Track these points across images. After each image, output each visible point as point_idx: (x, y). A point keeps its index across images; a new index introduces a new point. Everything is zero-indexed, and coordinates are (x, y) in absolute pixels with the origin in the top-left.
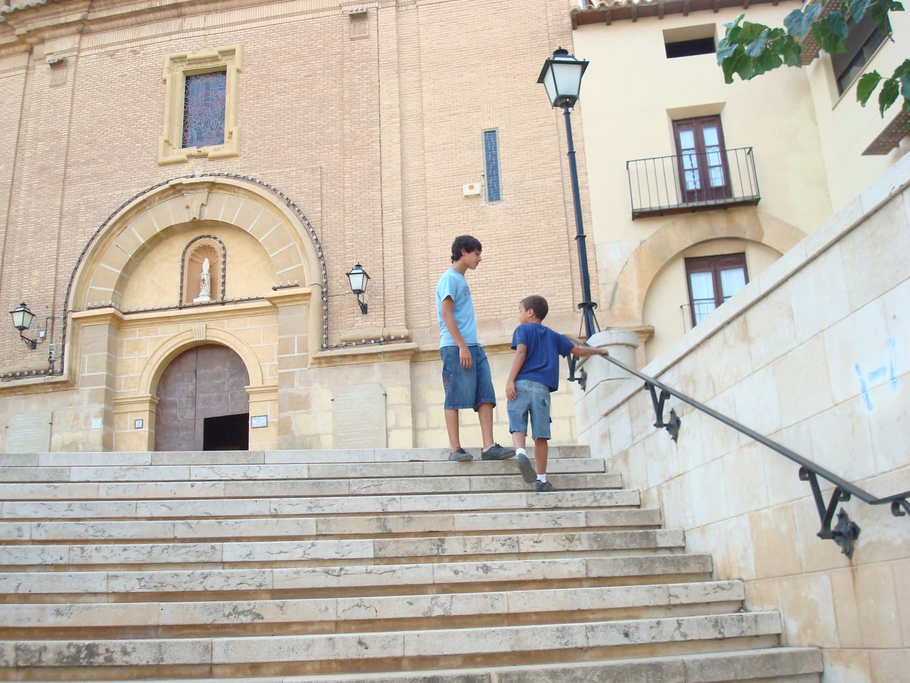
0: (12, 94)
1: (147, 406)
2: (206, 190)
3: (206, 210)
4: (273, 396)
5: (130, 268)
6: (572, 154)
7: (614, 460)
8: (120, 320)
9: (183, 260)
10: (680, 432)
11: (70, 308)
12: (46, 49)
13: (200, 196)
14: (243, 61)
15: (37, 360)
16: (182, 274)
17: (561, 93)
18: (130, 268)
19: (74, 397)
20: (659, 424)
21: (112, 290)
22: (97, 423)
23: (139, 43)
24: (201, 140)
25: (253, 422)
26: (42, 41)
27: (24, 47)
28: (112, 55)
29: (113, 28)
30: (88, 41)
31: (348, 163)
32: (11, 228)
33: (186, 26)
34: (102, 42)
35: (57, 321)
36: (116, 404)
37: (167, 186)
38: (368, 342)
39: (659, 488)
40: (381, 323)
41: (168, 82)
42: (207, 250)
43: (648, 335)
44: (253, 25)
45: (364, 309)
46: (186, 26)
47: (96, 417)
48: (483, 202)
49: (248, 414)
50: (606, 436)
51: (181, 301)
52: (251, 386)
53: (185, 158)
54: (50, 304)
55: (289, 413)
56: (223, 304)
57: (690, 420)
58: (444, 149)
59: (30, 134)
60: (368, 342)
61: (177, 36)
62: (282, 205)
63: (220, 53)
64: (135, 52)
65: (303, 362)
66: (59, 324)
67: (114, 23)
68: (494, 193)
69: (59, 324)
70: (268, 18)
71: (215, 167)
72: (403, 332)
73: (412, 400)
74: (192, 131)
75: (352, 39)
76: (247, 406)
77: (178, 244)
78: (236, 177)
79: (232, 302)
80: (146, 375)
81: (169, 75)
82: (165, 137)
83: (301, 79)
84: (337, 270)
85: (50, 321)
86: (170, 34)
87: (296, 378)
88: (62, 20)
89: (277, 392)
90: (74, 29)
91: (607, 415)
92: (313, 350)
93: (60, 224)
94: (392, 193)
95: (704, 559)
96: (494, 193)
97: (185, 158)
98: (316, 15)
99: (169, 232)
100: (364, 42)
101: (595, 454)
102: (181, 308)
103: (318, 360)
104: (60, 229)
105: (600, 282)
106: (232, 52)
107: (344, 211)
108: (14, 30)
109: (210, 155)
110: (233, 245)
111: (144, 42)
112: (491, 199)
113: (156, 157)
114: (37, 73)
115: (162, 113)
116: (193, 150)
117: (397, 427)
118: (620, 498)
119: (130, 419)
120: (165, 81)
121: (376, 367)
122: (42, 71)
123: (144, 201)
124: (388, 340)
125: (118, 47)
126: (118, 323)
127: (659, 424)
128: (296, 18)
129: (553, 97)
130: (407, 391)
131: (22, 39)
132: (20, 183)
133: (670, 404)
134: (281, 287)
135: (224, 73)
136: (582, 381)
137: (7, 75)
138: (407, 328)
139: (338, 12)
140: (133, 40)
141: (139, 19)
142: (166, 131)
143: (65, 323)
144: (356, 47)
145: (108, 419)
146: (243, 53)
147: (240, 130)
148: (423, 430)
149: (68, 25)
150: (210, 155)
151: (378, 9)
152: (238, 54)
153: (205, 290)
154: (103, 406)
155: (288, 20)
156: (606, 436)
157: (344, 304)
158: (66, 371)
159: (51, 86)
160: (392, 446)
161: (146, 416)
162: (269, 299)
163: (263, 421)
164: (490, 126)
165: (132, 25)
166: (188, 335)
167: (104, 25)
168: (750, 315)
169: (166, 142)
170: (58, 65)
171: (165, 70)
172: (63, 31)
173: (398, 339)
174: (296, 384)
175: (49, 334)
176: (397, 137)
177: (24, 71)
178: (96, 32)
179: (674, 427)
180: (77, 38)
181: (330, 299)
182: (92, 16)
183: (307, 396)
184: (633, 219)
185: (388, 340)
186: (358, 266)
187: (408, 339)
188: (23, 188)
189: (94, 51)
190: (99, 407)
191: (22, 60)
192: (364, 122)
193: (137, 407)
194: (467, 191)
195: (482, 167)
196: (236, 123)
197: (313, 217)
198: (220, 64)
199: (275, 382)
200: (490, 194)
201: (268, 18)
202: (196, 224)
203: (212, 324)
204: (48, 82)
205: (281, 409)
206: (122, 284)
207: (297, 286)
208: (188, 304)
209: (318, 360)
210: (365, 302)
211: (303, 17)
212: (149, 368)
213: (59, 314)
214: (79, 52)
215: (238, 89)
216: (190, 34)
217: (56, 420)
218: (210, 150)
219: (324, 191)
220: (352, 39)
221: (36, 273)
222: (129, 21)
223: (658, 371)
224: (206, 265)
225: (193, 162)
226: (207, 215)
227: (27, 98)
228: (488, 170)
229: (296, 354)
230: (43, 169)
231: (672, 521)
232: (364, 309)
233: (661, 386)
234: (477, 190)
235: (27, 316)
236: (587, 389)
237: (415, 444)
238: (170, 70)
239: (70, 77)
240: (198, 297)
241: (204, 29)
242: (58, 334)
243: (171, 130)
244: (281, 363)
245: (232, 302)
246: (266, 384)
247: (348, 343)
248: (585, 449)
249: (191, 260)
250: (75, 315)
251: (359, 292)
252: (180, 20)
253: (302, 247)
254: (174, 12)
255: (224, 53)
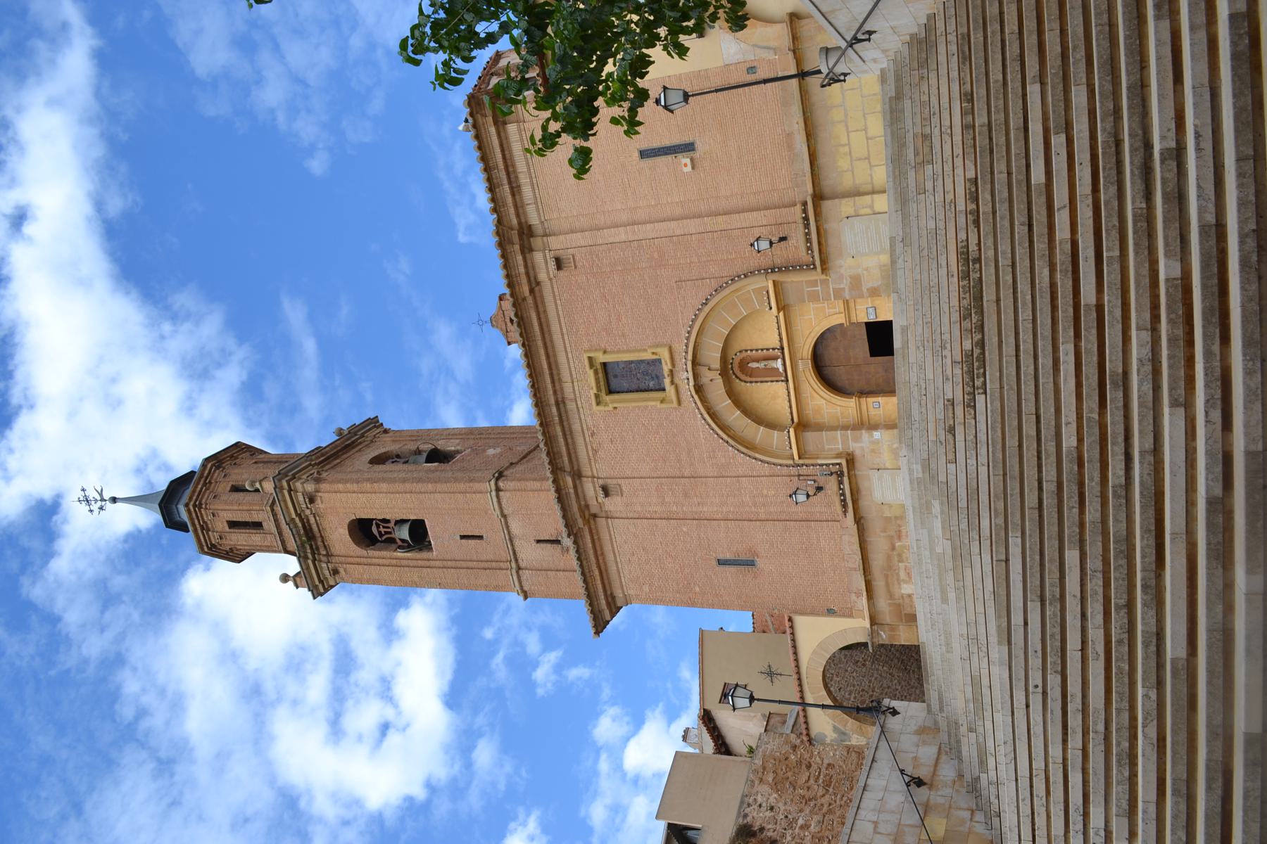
0: (628, 528)
1: (863, 400)
2: (698, 367)
3: (713, 366)
4: (852, 305)
5: (759, 420)
6: (717, 91)
7: (887, 56)
8: (799, 424)
9: (751, 382)
10: (873, 30)
11: (791, 462)
12: (593, 503)
13: (703, 371)
14: (596, 350)
15: (831, 484)
16: (762, 382)
17: (682, 100)
18: (759, 420)
19: (858, 453)
20: (869, 40)
21: (776, 432)
22: (877, 434)
23: (586, 432)
24: (658, 377)
25: (872, 318)
26: (587, 506)
27: (592, 522)
28: (595, 452)
29: (575, 452)
30: (586, 471)
31: (671, 262)
32: (731, 516)
33: (572, 396)
34: (587, 460)
35: (801, 473)
36: (862, 424)
37: (696, 397)
38: (808, 240)
39: (899, 36)
40: (794, 226)
41: (615, 405)
42: (743, 365)
43: (793, 18)
44: (568, 345)
45: (783, 239)
46: (572, 396)
47: (872, 436)
48: (697, 155)
49: (866, 323)
50: (875, 60)
51: (782, 381)
52: (844, 322)
53: (673, 386)
54: (788, 479)
55: (865, 290)
56: (782, 348)
57: (867, 27)
58: (656, 189)
59: (658, 509)
60: (808, 240)
61: (579, 403)
62: (707, 309)
63: (591, 368)
64: (593, 434)
65: (825, 282)
66: (804, 470)
67: (572, 451)
68: (688, 147)
69: (804, 470)
70: (562, 334)
71: (680, 362)
72: (799, 208)
73: (850, 197)
74: (651, 384)
75: (576, 267)
76: (859, 324)
77: (740, 386)
78: (687, 346)
79: (781, 340)
80: (839, 403)
81: (610, 405)
82: (658, 403)
83: (608, 304)
84: (756, 261)
85: (801, 478)
86: (578, 408)
87: (837, 286)
88: (572, 491)
89: (847, 301)
90: (578, 482)
91: (864, 61)
92: (817, 275)
93: (727, 477)
94: (692, 226)
95: (929, 17)
96: (688, 147)
97: (673, 386)
98: (557, 298)
99: (731, 393)
100: (577, 258)
101: (885, 65)
102: (787, 381)
103: (824, 270)
104: (731, 477)
105: (753, 58)
106: (590, 359)
107: (708, 261)
108: (579, 528)
109: (670, 368)
110: (739, 344)
111: (585, 426)
112: (694, 150)
113: (675, 408)
114: (611, 508)
115: (639, 407)
116: (667, 381)
117: (871, 207)
118: (906, 52)
119: (873, 412)
120: (615, 408)
121: (827, 226)
122: (613, 505)
123: (708, 413)
124: (806, 219)
125: (589, 447)
126: (802, 426)
127: (869, 40)
128: (561, 313)
129: (684, 104)
130: (844, 201)
131: (587, 522)
132: (696, 513)
133: (860, 36)
134: (769, 303)
135: (604, 365)
136: (845, 75)
137: (612, 533)
138: (796, 205)
139: (554, 281)
140: (584, 436)
141: (568, 433)
142: (653, 403)
143: (803, 465)
144: (581, 264)
145: (873, 427)
146: (590, 351)
147: (650, 347)
148: (873, 187)
149: (575, 487)
150: (670, 368)
151: (550, 250)
152: (591, 355)
153: (773, 364)
154: (864, 431)
155: (562, 319)
156: (875, 60)
157: (781, 254)
158: (838, 461)
159: (622, 496)
160: (886, 209)
161: (871, 400)
162: (779, 311)
163: (871, 310)
164: (637, 154)
165: (572, 438)
166: (808, 374)
167: (574, 459)
168: (823, 10)
169: (662, 402)
170: (606, 491)
171: (607, 408)
172: (579, 491)
173: (805, 211)
174: (842, 286)
175: (811, 478)
176: (649, 226)
177: (609, 520)
178: (579, 466)
179: (870, 33)
180: (584, 479)
181: (776, 265)
182: (567, 468)
183: (851, 277)
184: (703, 37)
185: (806, 219)
186: (752, 245)
187: (805, 204)
188: (700, 509)
189: (593, 466)
190: (865, 434)
191: (601, 522)
192: (639, 252)
193: (864, 407)
194: (689, 168)
195: (670, 158)
196: (645, 350)
197: (714, 284)
198: (599, 367)
199: (841, 302)
200: (689, 151)
201: (562, 334)
202: (724, 373)
203: (799, 355)
204: (619, 498)
205: (861, 296)
206: (772, 425)
207: (768, 292)
208: (784, 375)
209: (824, 270)
210: (777, 239)
211: (560, 308)
212: (834, 401)
213: (793, 471)
214: (594, 477)
215: (619, 352)
216: (577, 392)
217: (876, 467)
218: (666, 368)
219: (694, 278)
220: (576, 267)
221: (765, 492)
222: (570, 441)
223: (844, 41)
224: (754, 365)
225: (677, 380)
226: (717, 364)
227: (631, 515)
228: (671, 154)
229: (812, 317)
230: (686, 495)
231: (915, 30)
232: (783, 239)
233: (852, 40)
234: (688, 161)
235: (798, 492)
236: (850, 72)
237: (884, 192)
238: (606, 405)
239: (614, 481)
240: (778, 369)
241: (573, 383)
242: (811, 470)
243: (653, 400)
244: (827, 298)
245: (781, 340)
246: (843, 310)
247: (810, 248)
248: (882, 71)
249: (750, 376)
250: (796, 457)
251: (771, 243)
252: (567, 402)
253: (737, 290)
254: (561, 406)
255: (592, 365)
